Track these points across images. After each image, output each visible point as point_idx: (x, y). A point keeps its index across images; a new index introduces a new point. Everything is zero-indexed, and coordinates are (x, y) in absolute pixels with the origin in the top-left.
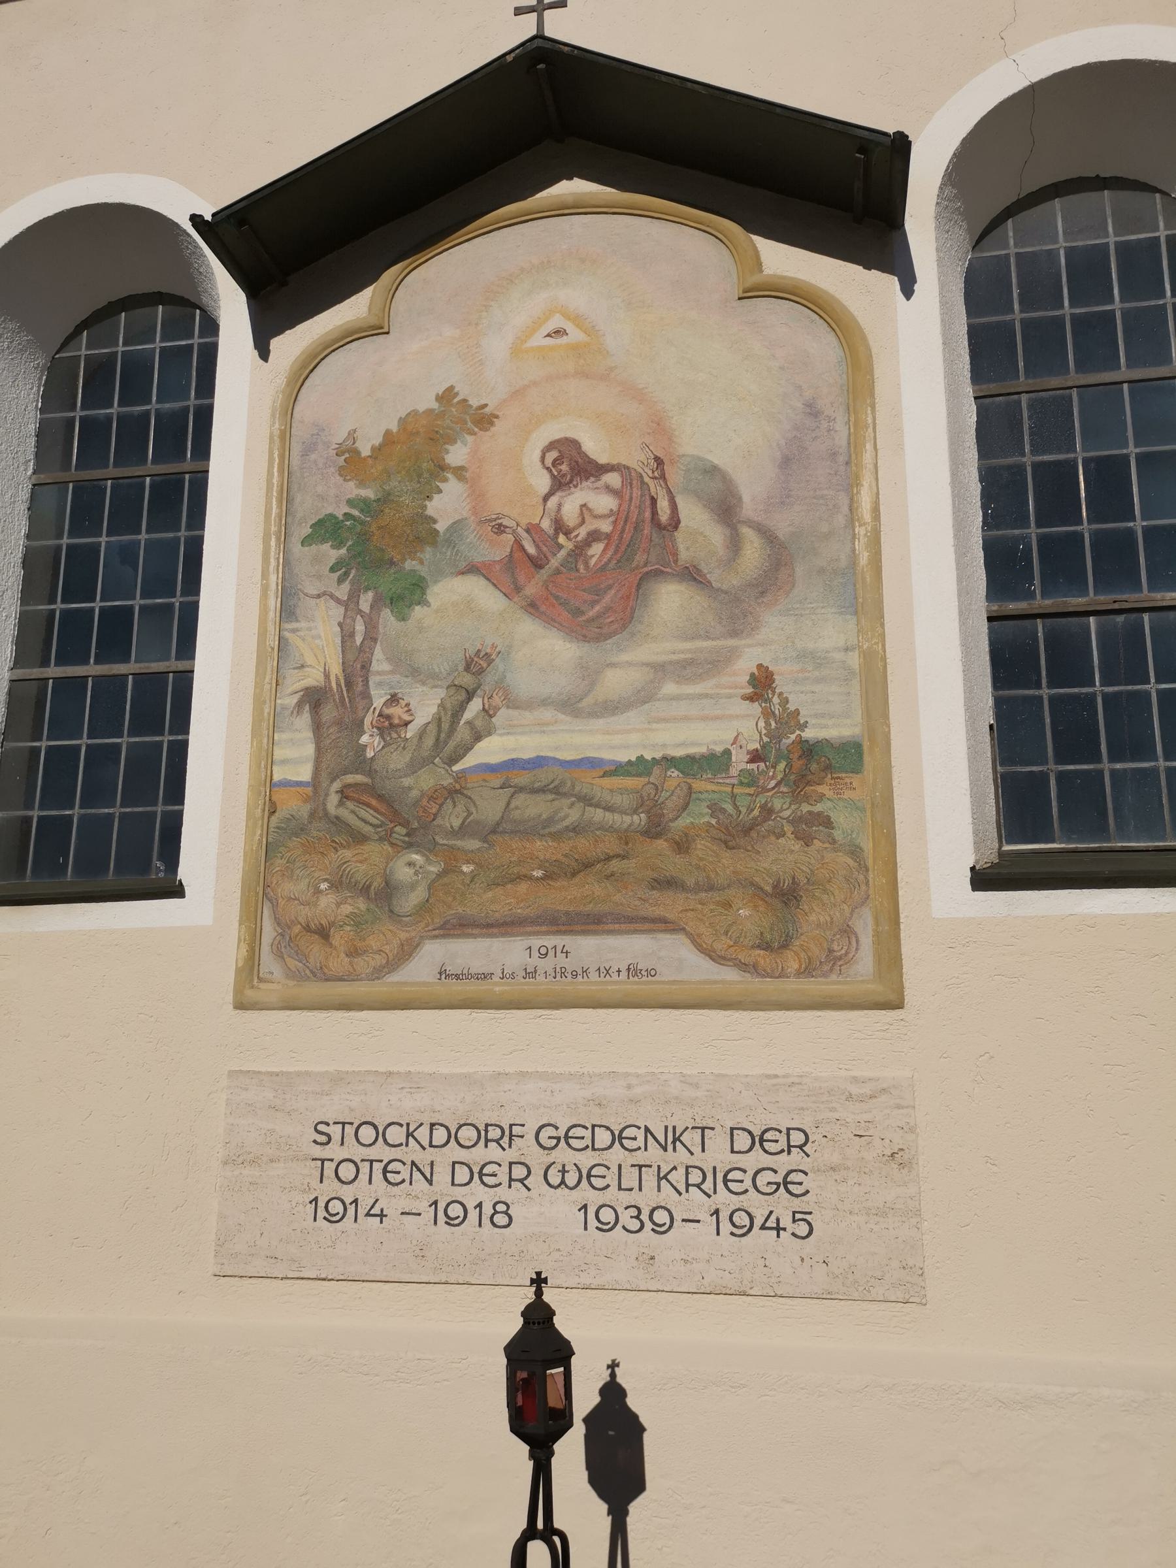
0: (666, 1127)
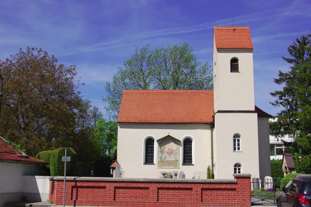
0: (239, 149)
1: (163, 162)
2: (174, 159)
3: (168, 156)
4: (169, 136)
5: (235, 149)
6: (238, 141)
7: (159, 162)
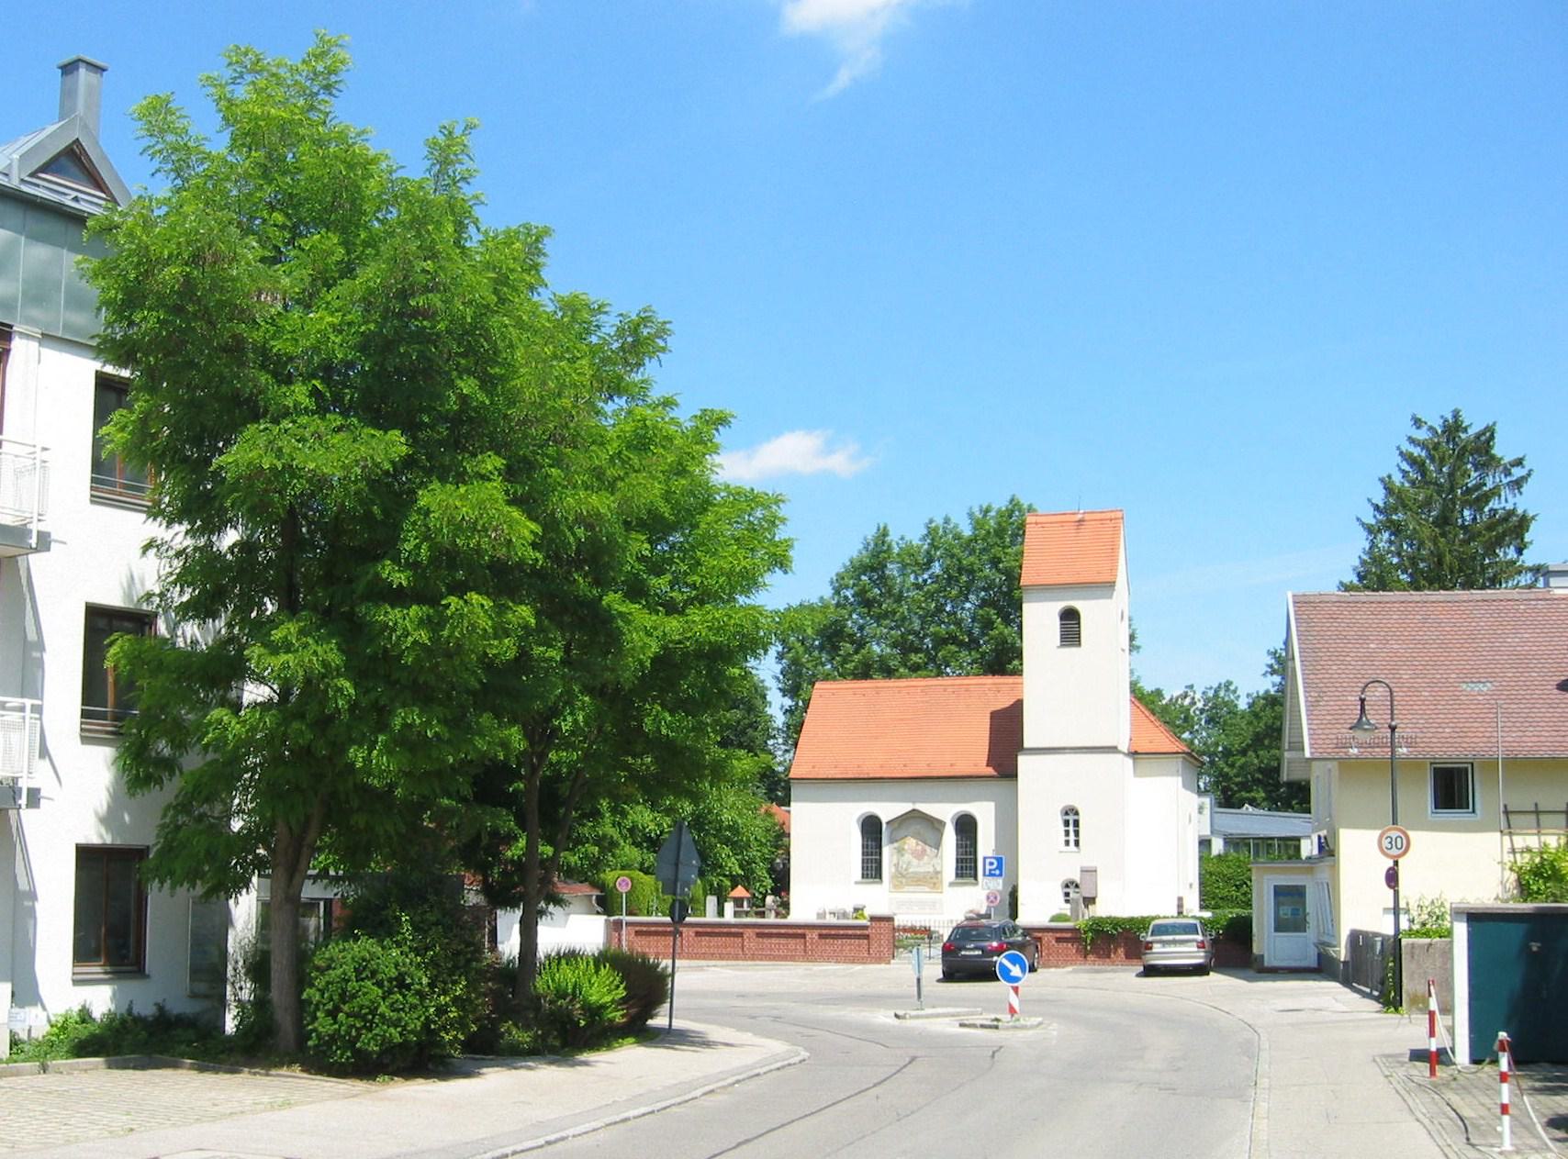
0: (1077, 843)
1: (903, 876)
2: (931, 870)
3: (915, 862)
4: (914, 810)
5: (1067, 843)
6: (1076, 823)
7: (893, 877)
